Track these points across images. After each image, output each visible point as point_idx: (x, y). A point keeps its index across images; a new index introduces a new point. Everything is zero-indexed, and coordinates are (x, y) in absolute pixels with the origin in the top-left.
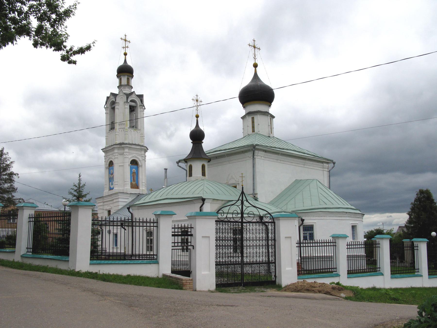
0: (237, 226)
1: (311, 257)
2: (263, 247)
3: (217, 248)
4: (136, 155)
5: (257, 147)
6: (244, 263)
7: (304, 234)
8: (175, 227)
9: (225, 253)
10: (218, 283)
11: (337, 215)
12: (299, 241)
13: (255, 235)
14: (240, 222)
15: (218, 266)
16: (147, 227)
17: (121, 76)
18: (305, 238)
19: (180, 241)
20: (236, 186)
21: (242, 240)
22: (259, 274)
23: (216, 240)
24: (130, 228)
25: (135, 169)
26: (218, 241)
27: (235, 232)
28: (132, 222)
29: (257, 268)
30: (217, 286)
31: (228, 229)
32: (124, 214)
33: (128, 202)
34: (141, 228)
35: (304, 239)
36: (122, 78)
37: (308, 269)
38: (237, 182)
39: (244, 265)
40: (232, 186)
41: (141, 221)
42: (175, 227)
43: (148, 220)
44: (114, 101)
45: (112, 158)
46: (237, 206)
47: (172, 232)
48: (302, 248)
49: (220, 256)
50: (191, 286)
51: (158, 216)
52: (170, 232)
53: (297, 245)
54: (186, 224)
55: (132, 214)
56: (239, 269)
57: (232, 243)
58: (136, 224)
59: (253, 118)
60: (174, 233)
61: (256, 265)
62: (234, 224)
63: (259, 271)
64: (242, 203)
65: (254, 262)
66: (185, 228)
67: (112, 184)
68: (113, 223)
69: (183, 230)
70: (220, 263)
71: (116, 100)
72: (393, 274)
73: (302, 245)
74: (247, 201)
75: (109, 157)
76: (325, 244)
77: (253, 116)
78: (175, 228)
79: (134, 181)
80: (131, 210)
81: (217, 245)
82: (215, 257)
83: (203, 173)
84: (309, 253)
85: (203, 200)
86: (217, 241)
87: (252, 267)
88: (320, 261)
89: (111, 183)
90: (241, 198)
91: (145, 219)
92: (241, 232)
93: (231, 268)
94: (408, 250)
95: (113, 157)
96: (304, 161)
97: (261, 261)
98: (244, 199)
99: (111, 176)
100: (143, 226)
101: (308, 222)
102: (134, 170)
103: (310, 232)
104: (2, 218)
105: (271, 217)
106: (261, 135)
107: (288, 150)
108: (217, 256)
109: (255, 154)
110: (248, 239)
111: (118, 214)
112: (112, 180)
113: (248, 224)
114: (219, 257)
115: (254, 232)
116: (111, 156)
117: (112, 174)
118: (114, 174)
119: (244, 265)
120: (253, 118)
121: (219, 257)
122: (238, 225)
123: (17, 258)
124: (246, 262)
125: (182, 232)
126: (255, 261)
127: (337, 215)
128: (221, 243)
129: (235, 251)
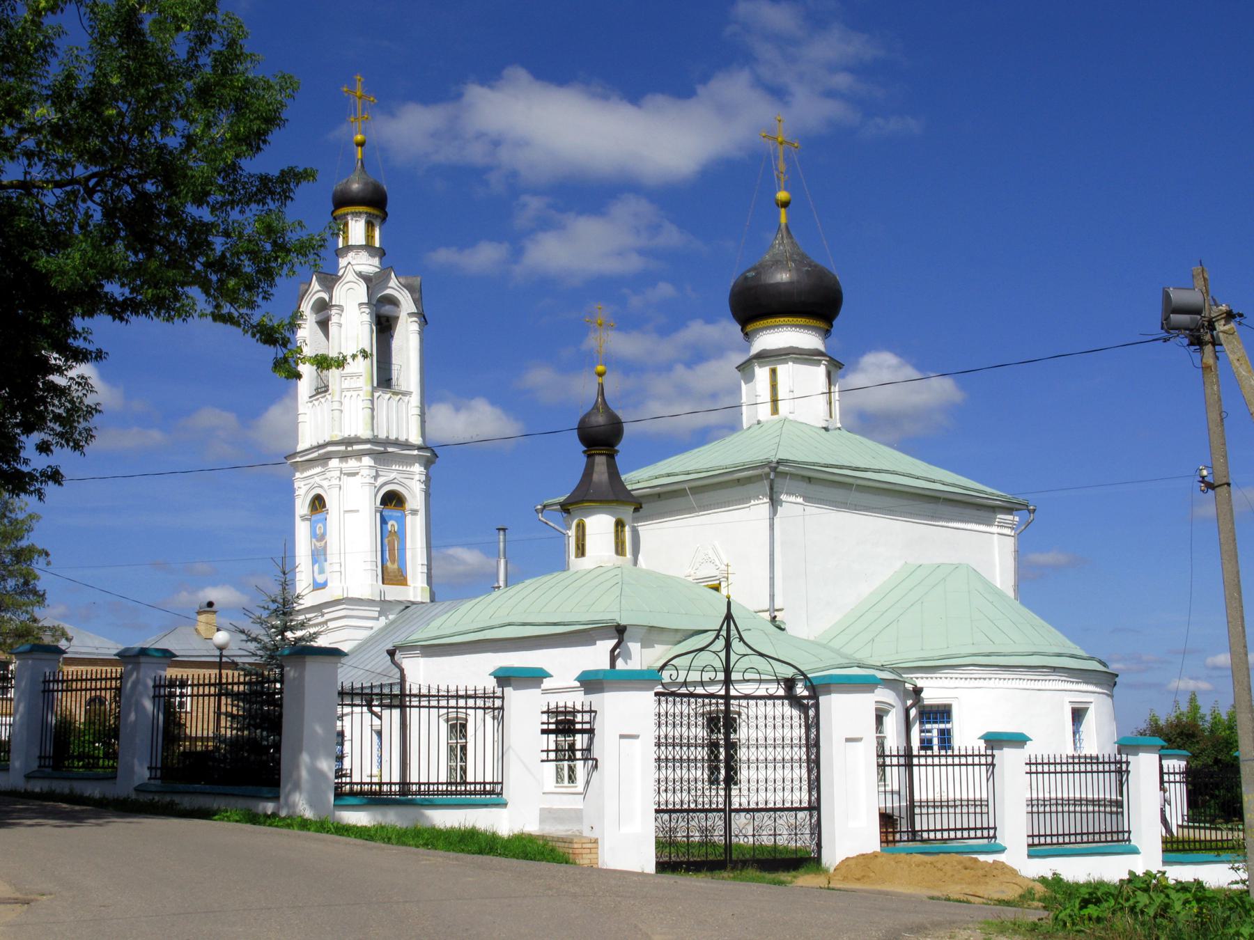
0: (712, 709)
1: (948, 801)
3: (659, 765)
4: (398, 476)
5: (781, 468)
7: (922, 731)
9: (682, 779)
10: (661, 860)
11: (1023, 677)
13: (764, 731)
14: (721, 697)
15: (662, 814)
16: (450, 710)
17: (347, 214)
18: (926, 744)
19: (552, 746)
21: (731, 746)
22: (773, 840)
23: (658, 745)
24: (396, 713)
25: (397, 522)
26: (663, 748)
27: (712, 722)
28: (403, 695)
29: (769, 822)
31: (689, 715)
32: (383, 671)
33: (375, 629)
34: (434, 711)
35: (922, 748)
36: (350, 221)
39: (733, 814)
40: (706, 584)
41: (460, 693)
43: (480, 692)
44: (327, 299)
45: (321, 486)
46: (714, 652)
47: (543, 723)
49: (667, 788)
50: (594, 856)
51: (505, 678)
52: (538, 720)
54: (577, 699)
55: (402, 671)
56: (720, 823)
57: (702, 753)
58: (410, 701)
59: (774, 372)
60: (545, 727)
61: (766, 814)
62: (707, 701)
63: (775, 830)
64: (728, 646)
66: (565, 713)
67: (322, 571)
68: (420, 701)
69: (561, 718)
71: (331, 298)
72: (1172, 851)
74: (741, 639)
75: (312, 481)
76: (1040, 768)
78: (1030, 764)
79: (393, 561)
80: (397, 657)
81: (659, 757)
82: (655, 790)
84: (937, 789)
85: (621, 631)
86: (659, 748)
87: (754, 819)
88: (962, 813)
89: (316, 566)
90: (724, 633)
92: (730, 723)
93: (696, 820)
95: (325, 484)
96: (932, 506)
98: (733, 632)
99: (318, 544)
100: (439, 707)
101: (932, 696)
102: (392, 525)
103: (942, 726)
104: (65, 685)
105: (808, 684)
107: (879, 471)
108: (659, 789)
109: (775, 490)
110: (744, 742)
111: (367, 668)
112: (322, 557)
113: (744, 702)
114: (666, 791)
115: (761, 722)
116: (317, 479)
117: (322, 537)
118: (328, 537)
119: (733, 814)
120: (774, 372)
121: (666, 791)
122: (717, 704)
123: (122, 789)
125: (557, 723)
127: (1023, 677)
128: (671, 752)
129: (713, 781)
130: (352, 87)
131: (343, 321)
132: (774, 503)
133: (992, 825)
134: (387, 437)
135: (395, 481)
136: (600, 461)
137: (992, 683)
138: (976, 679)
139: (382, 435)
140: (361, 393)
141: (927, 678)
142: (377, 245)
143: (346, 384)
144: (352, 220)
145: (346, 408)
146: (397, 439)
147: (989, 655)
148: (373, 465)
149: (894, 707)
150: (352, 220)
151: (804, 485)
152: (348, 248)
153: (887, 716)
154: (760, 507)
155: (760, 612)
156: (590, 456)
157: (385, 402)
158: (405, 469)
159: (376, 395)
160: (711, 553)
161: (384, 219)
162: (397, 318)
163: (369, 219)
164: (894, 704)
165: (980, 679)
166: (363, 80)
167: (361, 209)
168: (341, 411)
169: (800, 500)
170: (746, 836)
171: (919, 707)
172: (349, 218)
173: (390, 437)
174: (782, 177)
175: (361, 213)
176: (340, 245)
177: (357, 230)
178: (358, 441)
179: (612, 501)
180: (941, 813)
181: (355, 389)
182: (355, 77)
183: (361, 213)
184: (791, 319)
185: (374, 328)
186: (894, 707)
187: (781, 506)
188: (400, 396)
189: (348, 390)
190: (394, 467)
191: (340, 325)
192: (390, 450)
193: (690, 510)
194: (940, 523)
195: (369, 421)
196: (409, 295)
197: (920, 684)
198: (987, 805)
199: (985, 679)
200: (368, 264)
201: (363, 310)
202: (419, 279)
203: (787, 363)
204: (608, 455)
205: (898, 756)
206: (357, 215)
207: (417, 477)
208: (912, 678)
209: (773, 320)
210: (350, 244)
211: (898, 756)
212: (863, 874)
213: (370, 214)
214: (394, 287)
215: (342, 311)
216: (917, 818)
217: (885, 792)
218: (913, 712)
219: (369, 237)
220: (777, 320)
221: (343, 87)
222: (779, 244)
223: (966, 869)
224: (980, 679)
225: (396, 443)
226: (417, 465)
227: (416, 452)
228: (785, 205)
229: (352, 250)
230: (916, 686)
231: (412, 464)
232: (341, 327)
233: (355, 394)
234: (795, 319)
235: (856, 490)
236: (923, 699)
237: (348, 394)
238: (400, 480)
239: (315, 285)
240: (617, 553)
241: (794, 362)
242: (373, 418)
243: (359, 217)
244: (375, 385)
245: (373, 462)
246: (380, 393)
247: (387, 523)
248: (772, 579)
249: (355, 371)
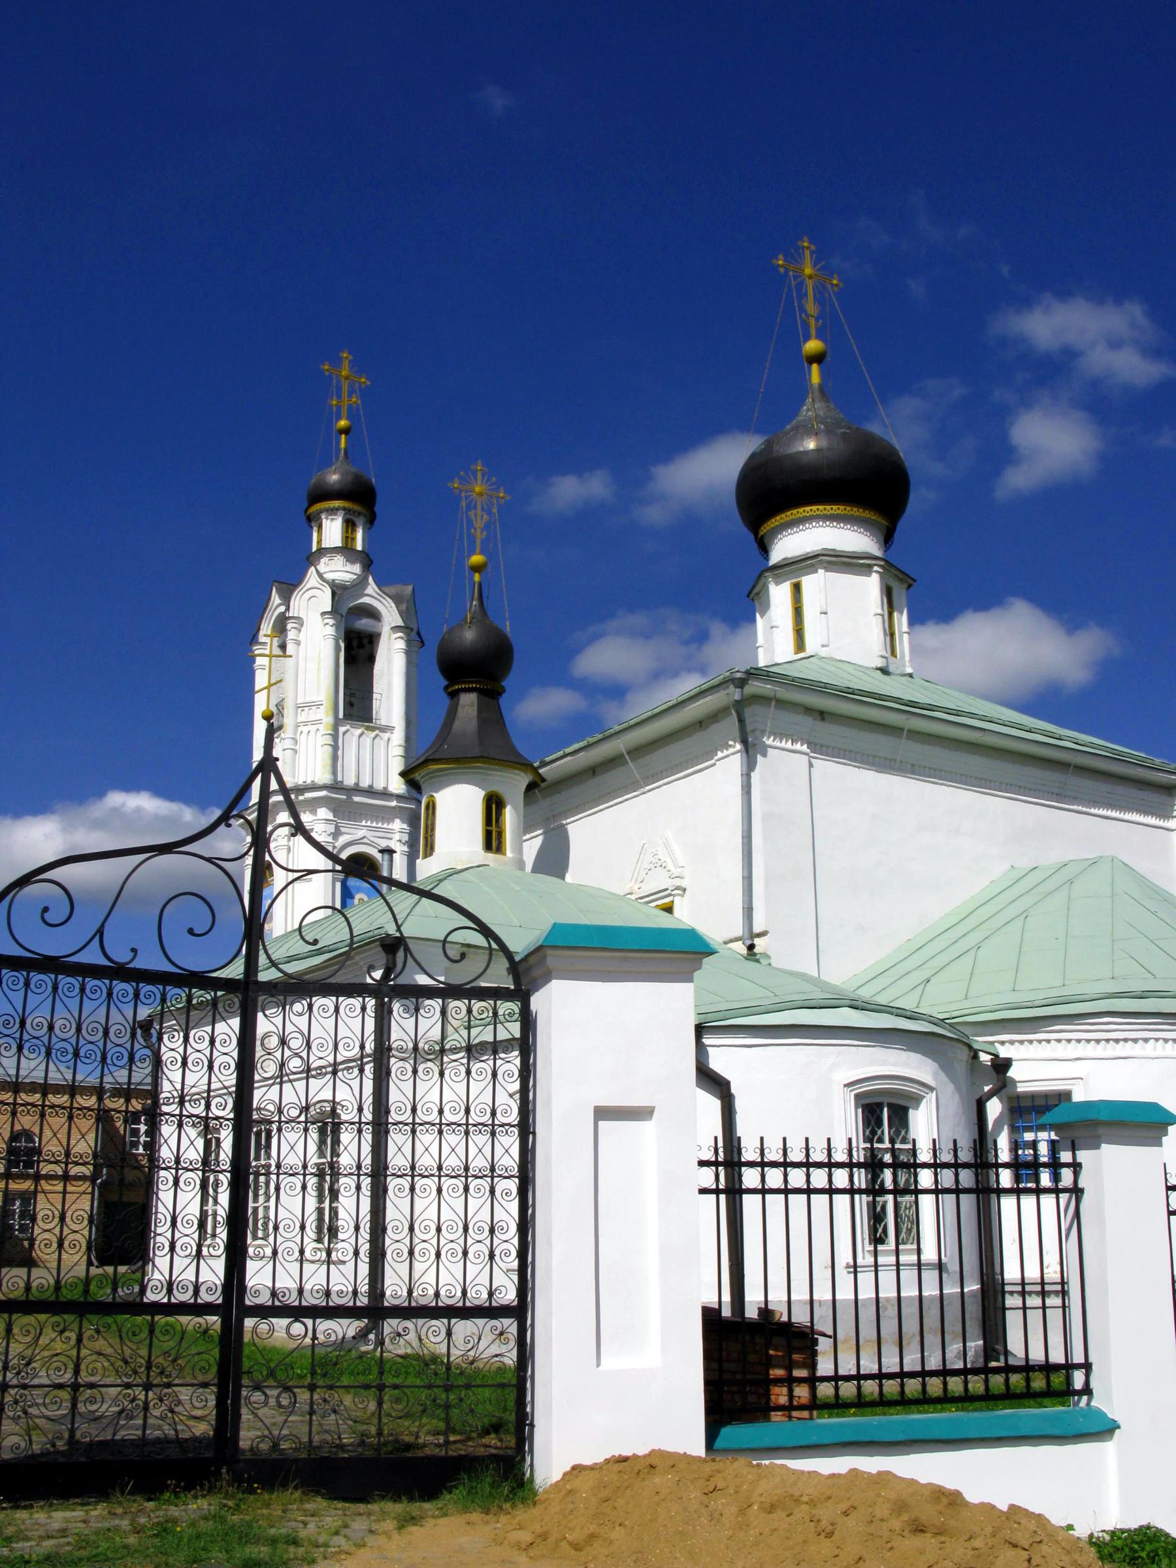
2: (185, 1176)
4: (369, 834)
6: (248, 1302)
8: (807, 1155)
12: (720, 1144)
20: (673, 902)
30: (486, 1404)
36: (324, 521)
37: (1037, 1355)
38: (678, 882)
42: (807, 1155)
48: (751, 1204)
53: (707, 1177)
59: (797, 588)
65: (335, 1300)
70: (170, 1291)
73: (750, 1177)
77: (795, 580)
83: (488, 836)
91: (819, 1149)
94: (66, 1172)
97: (340, 1293)
106: (836, 660)
110: (294, 1113)
124: (264, 1299)
126: (294, 1286)
130: (337, 362)
131: (302, 637)
132: (751, 750)
133: (1078, 1358)
134: (357, 784)
135: (365, 840)
136: (469, 701)
137: (1150, 1049)
138: (1117, 1041)
139: (350, 781)
140: (321, 727)
141: (1021, 1042)
142: (359, 547)
143: (302, 717)
144: (327, 519)
145: (302, 747)
146: (371, 787)
147: (1142, 996)
148: (331, 817)
149: (931, 1089)
150: (327, 519)
151: (807, 721)
152: (322, 551)
153: (917, 1108)
154: (730, 762)
155: (731, 941)
156: (454, 695)
157: (355, 739)
158: (380, 825)
159: (342, 729)
160: (663, 855)
161: (371, 520)
162: (379, 635)
163: (348, 517)
164: (932, 1083)
165: (1126, 1040)
166: (351, 357)
167: (337, 504)
168: (295, 751)
169: (805, 748)
170: (287, 1389)
171: (1010, 1099)
172: (323, 516)
173: (361, 785)
174: (812, 321)
175: (337, 509)
176: (314, 549)
177: (332, 531)
178: (314, 787)
179: (476, 759)
180: (1024, 1308)
181: (314, 722)
182: (341, 354)
183: (337, 509)
184: (821, 507)
185: (342, 645)
186: (931, 1089)
187: (764, 755)
188: (377, 732)
189: (306, 723)
190: (364, 823)
191: (298, 643)
192: (357, 799)
193: (631, 786)
194: (1075, 807)
195: (329, 761)
196: (393, 605)
197: (1004, 1052)
198: (1064, 1293)
199: (1135, 1041)
200: (340, 570)
201: (327, 621)
202: (411, 587)
203: (816, 572)
204: (480, 692)
205: (850, 1165)
206: (332, 511)
207: (397, 836)
208: (992, 1043)
209: (795, 511)
210: (323, 546)
211: (850, 1165)
212: (592, 1528)
213: (349, 510)
214: (372, 595)
215: (302, 625)
216: (1013, 1321)
217: (919, 1265)
218: (994, 1108)
219: (348, 538)
220: (801, 510)
221: (324, 365)
222: (808, 410)
223: (919, 1529)
224: (1126, 1040)
225: (370, 792)
226: (397, 821)
227: (394, 803)
228: (818, 358)
229: (325, 556)
230: (996, 1056)
231: (390, 820)
232: (299, 645)
233: (313, 728)
234: (828, 507)
235: (908, 738)
236: (1014, 1082)
237: (305, 729)
238: (372, 839)
239: (276, 599)
240: (488, 846)
241: (827, 570)
242: (335, 758)
243: (336, 514)
244: (341, 715)
245: (331, 814)
246: (348, 727)
247: (352, 897)
248: (748, 879)
249: (314, 699)
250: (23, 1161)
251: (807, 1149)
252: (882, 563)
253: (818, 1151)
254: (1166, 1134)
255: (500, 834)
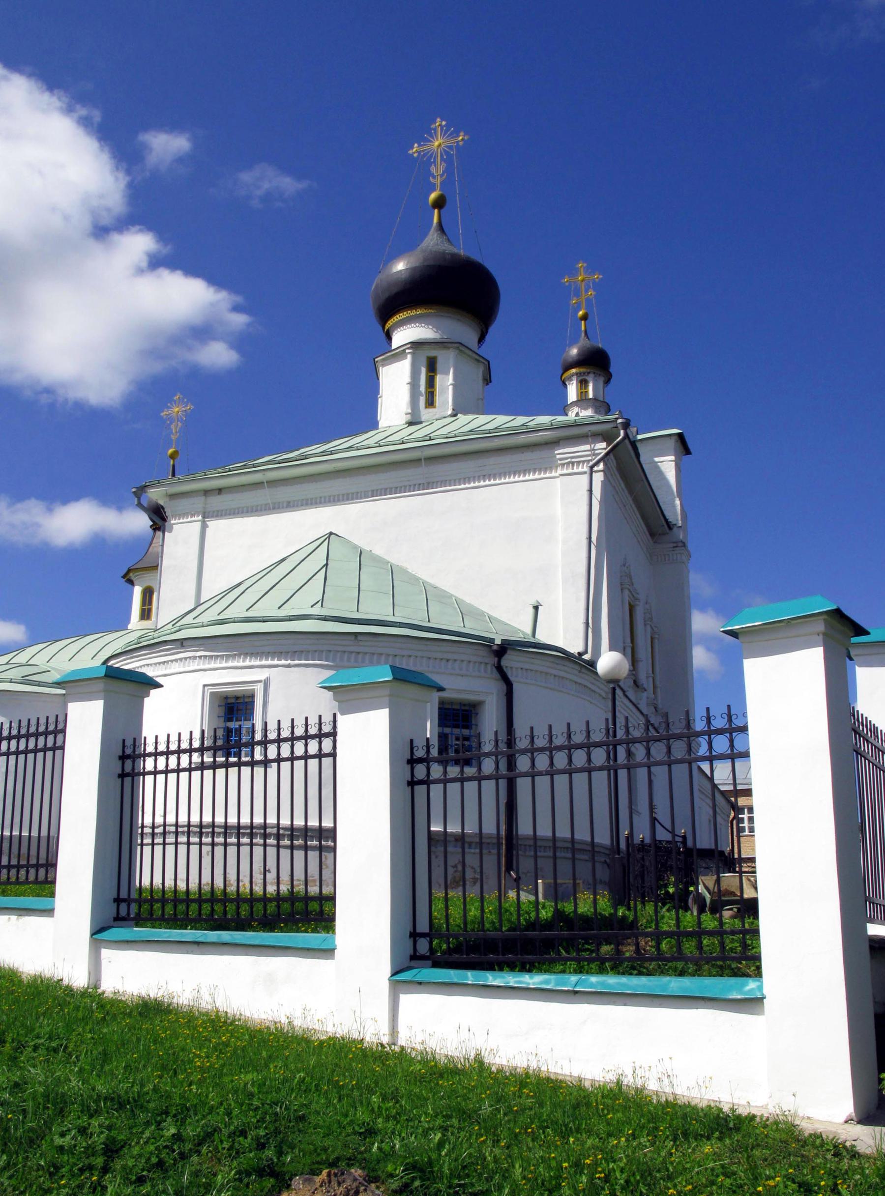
42: (551, 740)
48: (523, 785)
213: (580, 374)
250: (18, 1118)
251: (588, 732)
252: (409, 346)
253: (718, 717)
254: (148, 696)
255: (150, 610)
